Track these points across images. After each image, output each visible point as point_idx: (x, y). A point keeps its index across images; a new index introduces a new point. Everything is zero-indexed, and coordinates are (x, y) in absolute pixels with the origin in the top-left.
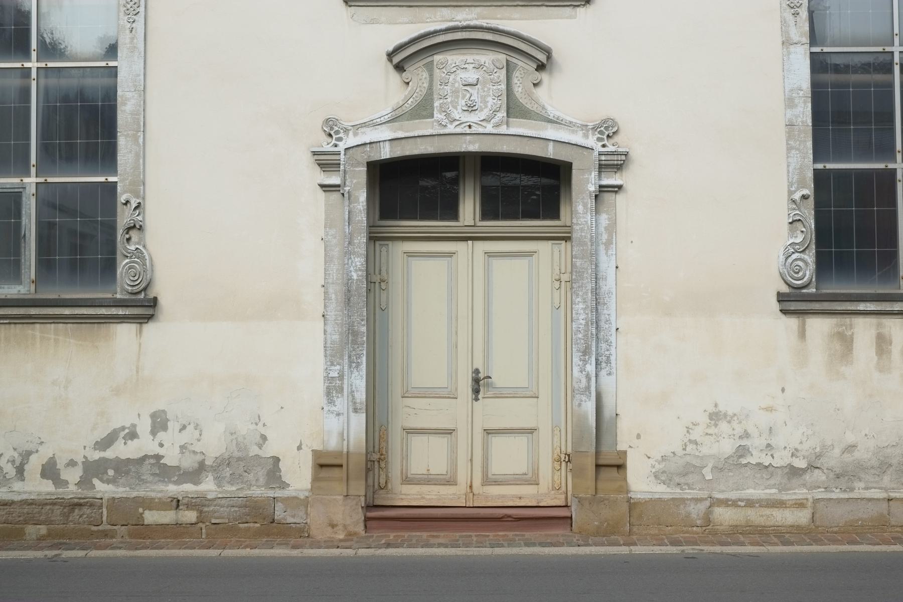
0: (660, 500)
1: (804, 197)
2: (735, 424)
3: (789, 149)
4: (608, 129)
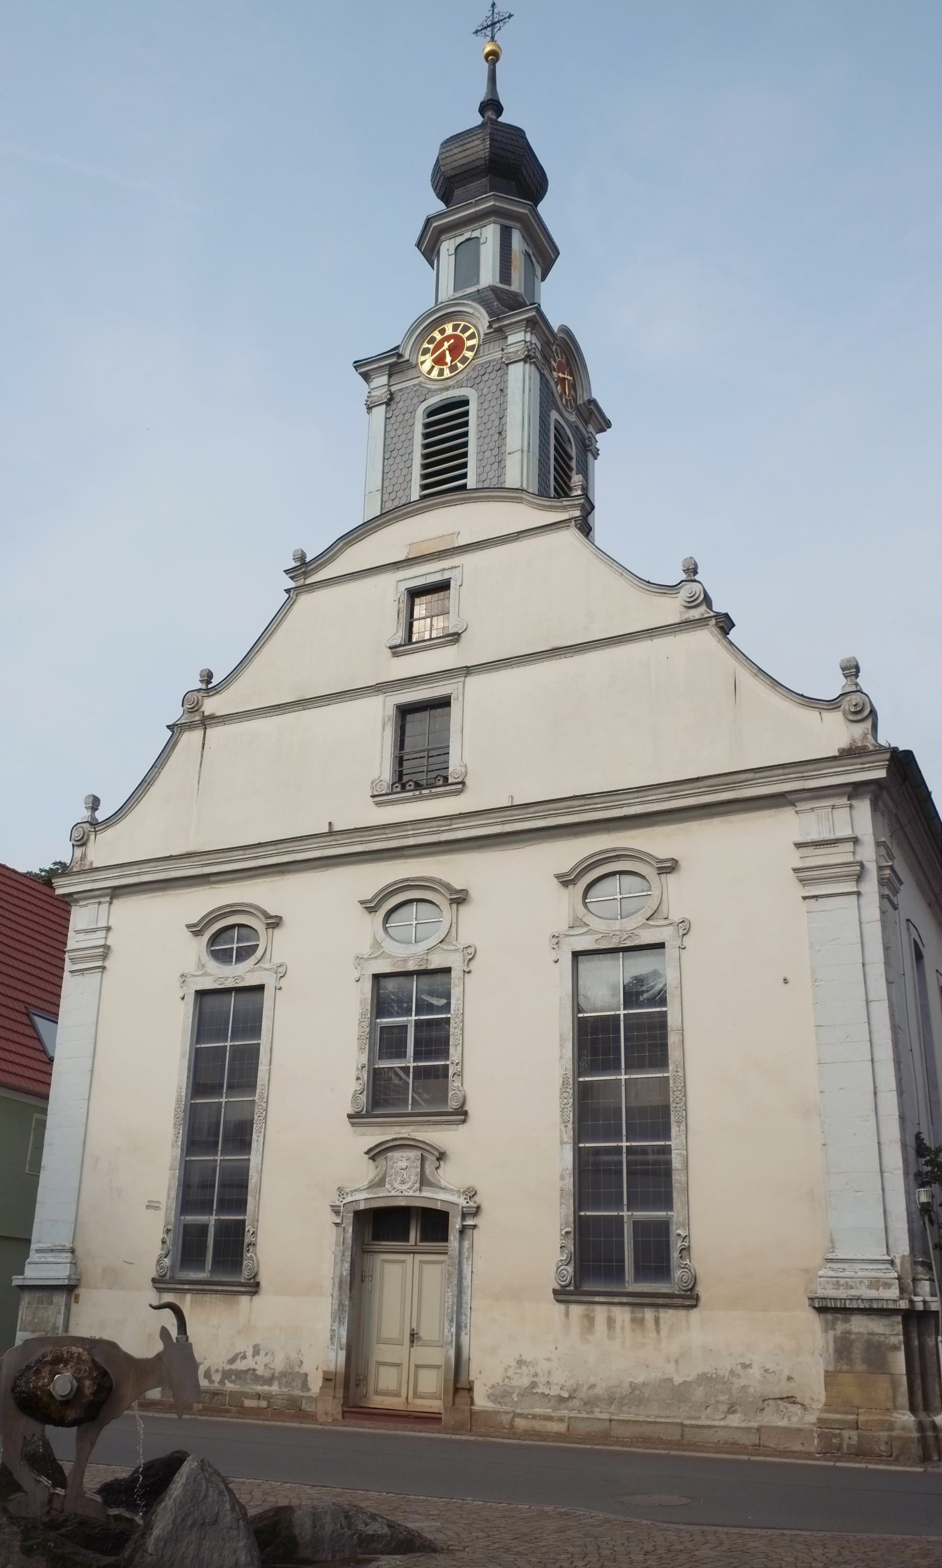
0: (487, 1411)
1: (567, 1233)
2: (530, 1368)
3: (561, 1204)
4: (471, 1194)
